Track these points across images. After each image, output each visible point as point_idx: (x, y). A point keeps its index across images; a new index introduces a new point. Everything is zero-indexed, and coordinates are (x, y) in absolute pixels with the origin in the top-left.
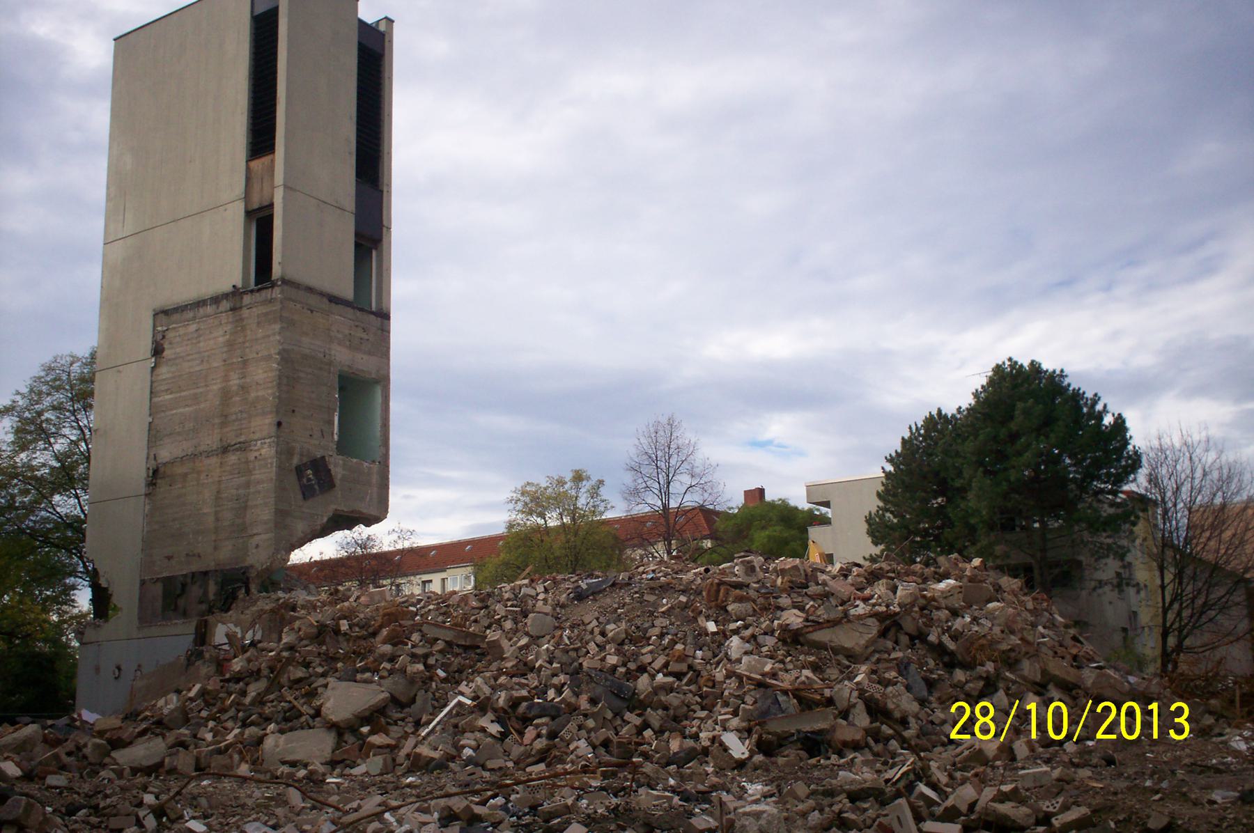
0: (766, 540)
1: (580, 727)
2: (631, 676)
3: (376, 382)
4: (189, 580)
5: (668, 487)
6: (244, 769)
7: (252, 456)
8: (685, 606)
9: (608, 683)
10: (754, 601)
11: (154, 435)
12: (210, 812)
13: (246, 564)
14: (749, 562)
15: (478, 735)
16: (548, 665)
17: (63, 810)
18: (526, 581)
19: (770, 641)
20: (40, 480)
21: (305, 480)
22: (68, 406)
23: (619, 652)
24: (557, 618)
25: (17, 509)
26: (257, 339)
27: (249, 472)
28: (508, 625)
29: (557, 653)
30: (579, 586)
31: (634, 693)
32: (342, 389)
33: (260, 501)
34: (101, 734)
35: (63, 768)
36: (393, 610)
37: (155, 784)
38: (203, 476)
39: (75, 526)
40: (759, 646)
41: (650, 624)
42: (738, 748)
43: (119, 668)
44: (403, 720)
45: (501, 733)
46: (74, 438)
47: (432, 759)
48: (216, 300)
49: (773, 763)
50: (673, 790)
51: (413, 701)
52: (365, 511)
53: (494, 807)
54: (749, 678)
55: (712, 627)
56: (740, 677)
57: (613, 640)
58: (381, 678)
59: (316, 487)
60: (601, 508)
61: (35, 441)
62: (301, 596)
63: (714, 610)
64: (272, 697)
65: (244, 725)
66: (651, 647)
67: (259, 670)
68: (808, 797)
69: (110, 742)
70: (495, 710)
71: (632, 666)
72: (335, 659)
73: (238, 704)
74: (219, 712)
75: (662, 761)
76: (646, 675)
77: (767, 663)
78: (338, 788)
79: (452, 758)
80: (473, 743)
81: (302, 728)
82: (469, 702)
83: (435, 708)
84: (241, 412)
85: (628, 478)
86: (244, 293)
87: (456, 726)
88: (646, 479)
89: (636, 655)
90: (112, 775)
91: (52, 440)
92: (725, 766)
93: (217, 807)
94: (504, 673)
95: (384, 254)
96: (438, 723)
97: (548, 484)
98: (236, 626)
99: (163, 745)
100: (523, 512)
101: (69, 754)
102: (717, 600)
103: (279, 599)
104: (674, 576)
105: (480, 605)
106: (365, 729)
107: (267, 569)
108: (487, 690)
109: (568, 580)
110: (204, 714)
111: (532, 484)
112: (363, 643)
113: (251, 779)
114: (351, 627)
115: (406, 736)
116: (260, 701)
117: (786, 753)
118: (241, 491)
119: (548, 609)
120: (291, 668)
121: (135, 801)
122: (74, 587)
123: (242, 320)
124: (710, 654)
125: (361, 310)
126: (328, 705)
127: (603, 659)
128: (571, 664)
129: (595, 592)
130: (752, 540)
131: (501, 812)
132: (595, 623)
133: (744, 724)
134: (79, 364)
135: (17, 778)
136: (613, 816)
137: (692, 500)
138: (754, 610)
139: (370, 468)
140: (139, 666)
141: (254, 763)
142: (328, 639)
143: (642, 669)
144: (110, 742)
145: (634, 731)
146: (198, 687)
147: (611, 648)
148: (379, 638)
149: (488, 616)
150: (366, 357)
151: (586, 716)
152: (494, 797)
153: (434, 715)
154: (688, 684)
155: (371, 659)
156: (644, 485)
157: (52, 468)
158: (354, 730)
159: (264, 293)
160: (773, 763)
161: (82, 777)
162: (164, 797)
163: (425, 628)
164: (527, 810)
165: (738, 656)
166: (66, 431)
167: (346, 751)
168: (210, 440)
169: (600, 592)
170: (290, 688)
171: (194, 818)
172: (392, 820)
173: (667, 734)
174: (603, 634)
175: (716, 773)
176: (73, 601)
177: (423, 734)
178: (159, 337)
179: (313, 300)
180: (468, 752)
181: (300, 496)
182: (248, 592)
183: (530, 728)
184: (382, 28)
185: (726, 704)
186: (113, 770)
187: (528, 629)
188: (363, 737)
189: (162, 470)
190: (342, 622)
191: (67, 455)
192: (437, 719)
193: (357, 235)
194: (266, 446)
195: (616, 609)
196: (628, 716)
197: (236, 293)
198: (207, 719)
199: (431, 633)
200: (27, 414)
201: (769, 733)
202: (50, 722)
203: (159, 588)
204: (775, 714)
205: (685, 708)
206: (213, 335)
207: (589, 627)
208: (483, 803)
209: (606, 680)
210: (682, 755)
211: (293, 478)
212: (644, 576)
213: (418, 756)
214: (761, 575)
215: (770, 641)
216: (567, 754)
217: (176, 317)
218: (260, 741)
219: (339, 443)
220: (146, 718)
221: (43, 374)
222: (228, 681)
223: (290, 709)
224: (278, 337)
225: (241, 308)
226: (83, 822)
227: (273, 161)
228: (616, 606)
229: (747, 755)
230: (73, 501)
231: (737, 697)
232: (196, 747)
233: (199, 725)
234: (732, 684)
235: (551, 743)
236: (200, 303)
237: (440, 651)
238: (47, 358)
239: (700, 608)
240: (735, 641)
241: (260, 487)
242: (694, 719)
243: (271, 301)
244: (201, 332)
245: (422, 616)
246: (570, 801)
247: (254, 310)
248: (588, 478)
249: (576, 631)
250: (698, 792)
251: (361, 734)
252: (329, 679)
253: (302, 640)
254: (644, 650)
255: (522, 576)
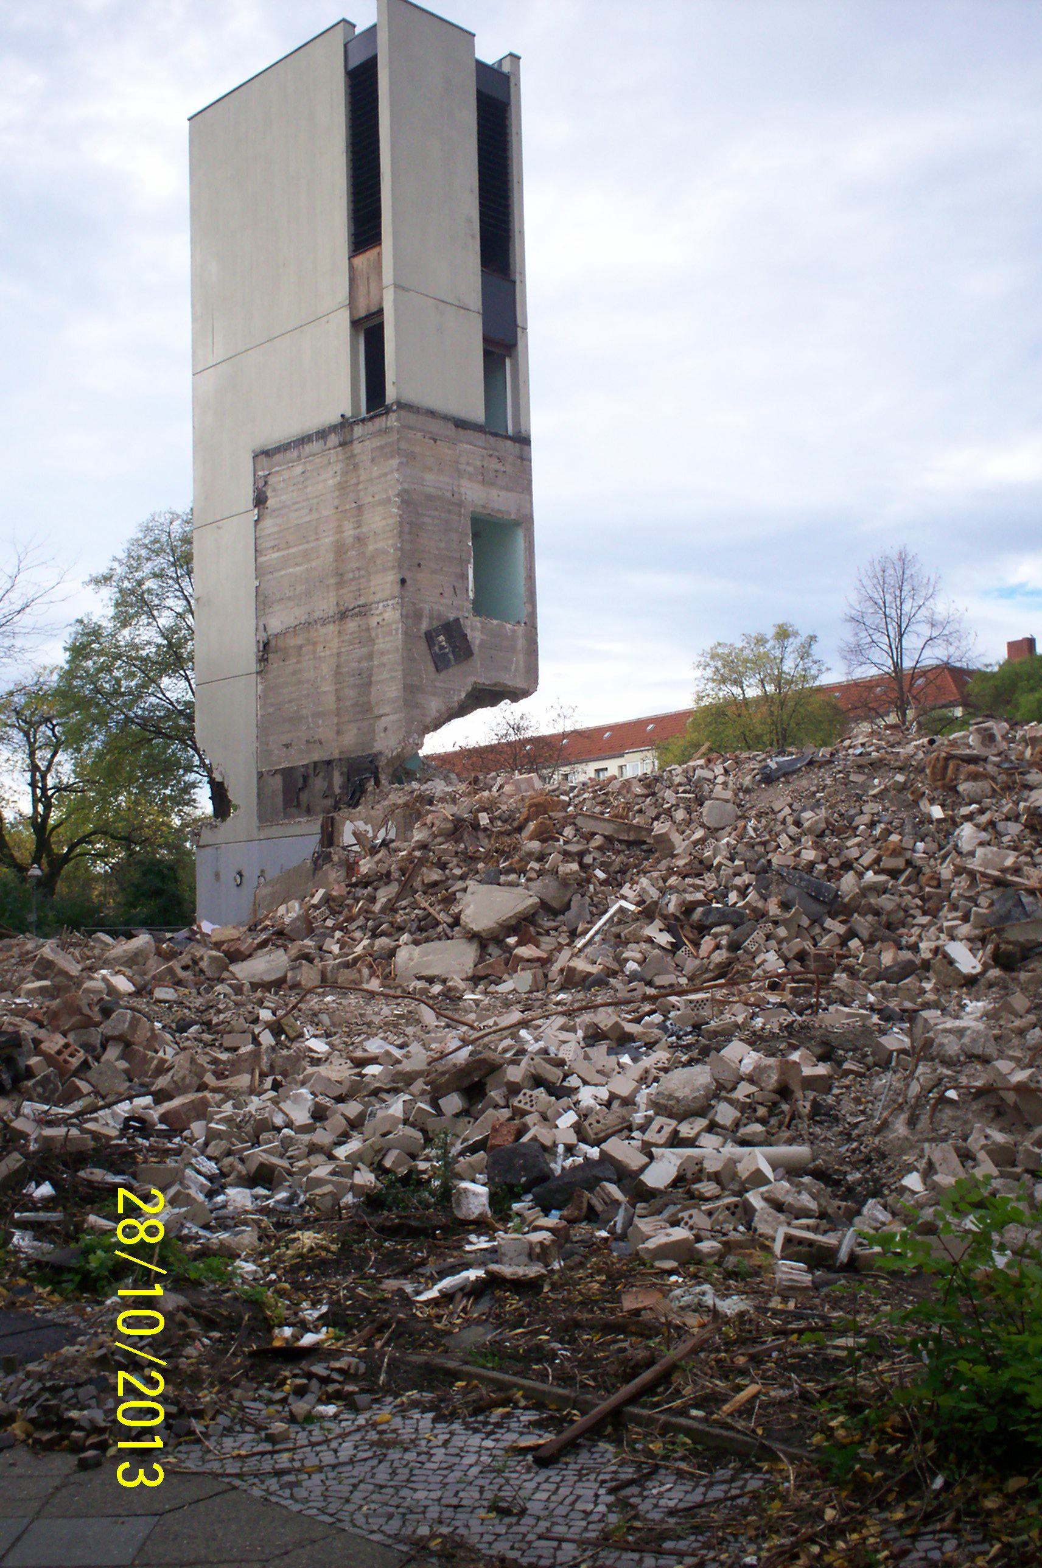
0: (1035, 705)
1: (768, 937)
2: (832, 874)
3: (517, 524)
4: (311, 771)
5: (900, 640)
6: (374, 985)
7: (373, 622)
8: (902, 788)
9: (803, 884)
10: (994, 779)
11: (263, 602)
12: (333, 1030)
13: (375, 751)
14: (986, 729)
15: (644, 946)
16: (729, 863)
17: (174, 1025)
18: (701, 762)
19: (1014, 829)
20: (145, 660)
21: (436, 648)
22: (171, 572)
23: (816, 846)
24: (739, 806)
25: (122, 694)
26: (371, 480)
27: (371, 641)
28: (680, 815)
29: (741, 848)
30: (767, 766)
31: (837, 896)
32: (476, 536)
33: (385, 675)
34: (217, 945)
35: (179, 983)
36: (541, 799)
37: (271, 1000)
38: (320, 648)
39: (187, 712)
40: (999, 835)
41: (857, 810)
42: (967, 961)
43: (240, 874)
44: (556, 929)
45: (672, 944)
46: (180, 610)
47: (589, 974)
48: (322, 434)
49: (1013, 979)
50: (872, 1008)
51: (568, 907)
52: (509, 683)
53: (650, 1025)
54: (983, 875)
55: (937, 812)
56: (972, 874)
57: (810, 831)
58: (529, 880)
59: (451, 656)
60: (813, 672)
61: (137, 614)
62: (438, 787)
63: (939, 791)
64: (404, 903)
65: (374, 936)
66: (858, 839)
67: (389, 874)
68: (1028, 1012)
69: (227, 953)
70: (664, 917)
71: (834, 862)
72: (473, 859)
73: (367, 912)
74: (346, 921)
75: (871, 977)
76: (851, 873)
77: (1008, 856)
78: (477, 1005)
79: (614, 974)
80: (639, 956)
81: (440, 939)
82: (632, 907)
83: (592, 914)
84: (358, 569)
85: (847, 635)
86: (356, 423)
87: (618, 936)
88: (871, 632)
89: (839, 849)
90: (229, 990)
91: (155, 613)
92: (950, 982)
93: (340, 1025)
94: (675, 873)
95: (520, 360)
96: (597, 933)
97: (744, 644)
98: (366, 823)
99: (285, 958)
100: (714, 680)
101: (185, 968)
102: (944, 778)
103: (412, 792)
104: (889, 750)
105: (645, 792)
106: (512, 940)
107: (398, 756)
108: (654, 893)
109: (754, 758)
110: (330, 923)
111: (725, 645)
112: (508, 840)
113: (381, 994)
114: (491, 820)
115: (559, 948)
116: (391, 908)
117: (1032, 966)
118: (365, 664)
119: (728, 794)
120: (424, 870)
121: (251, 1018)
122: (193, 785)
123: (353, 456)
124: (934, 846)
125: (495, 435)
126: (468, 912)
127: (797, 855)
128: (757, 861)
129: (786, 773)
130: (1017, 707)
131: (656, 1031)
132: (787, 810)
133: (977, 932)
134: (179, 522)
135: (130, 994)
136: (786, 1034)
137: (932, 657)
138: (994, 790)
139: (514, 631)
140: (262, 871)
141: (386, 977)
142: (466, 836)
143: (847, 866)
144: (227, 953)
145: (837, 941)
146: (321, 892)
147: (807, 841)
148: (526, 833)
149: (655, 804)
150: (503, 493)
151: (776, 923)
152: (650, 1013)
153: (592, 923)
154: (907, 882)
155: (517, 858)
156: (869, 640)
157: (158, 646)
158: (499, 941)
159: (377, 421)
160: (1013, 979)
161: (199, 993)
162: (280, 1013)
163: (579, 821)
164: (689, 1029)
165: (970, 848)
166: (170, 602)
167: (490, 965)
168: (325, 604)
169: (794, 772)
170: (425, 893)
171: (315, 1036)
172: (529, 1037)
173: (878, 946)
174: (798, 823)
175: (936, 990)
176: (194, 801)
177: (579, 945)
178: (261, 483)
179: (436, 426)
180: (632, 966)
181: (431, 667)
182: (377, 783)
183: (707, 938)
184: (506, 68)
185: (954, 908)
186: (230, 985)
187: (705, 820)
188: (509, 949)
189: (273, 643)
190: (481, 815)
191: (174, 630)
192: (596, 928)
193: (486, 340)
194: (389, 609)
195: (814, 793)
196: (829, 923)
197: (345, 424)
198: (334, 929)
199: (587, 826)
200: (126, 584)
201: (1008, 942)
202: (169, 935)
203: (277, 782)
204: (1018, 919)
205: (902, 913)
206: (321, 478)
207: (780, 816)
208: (638, 1021)
209: (801, 879)
210: (895, 969)
211: (423, 646)
212: (851, 751)
213: (572, 970)
214: (1004, 745)
215: (1014, 829)
216: (752, 968)
217: (278, 458)
218: (392, 953)
219: (475, 602)
220: (265, 928)
221: (140, 535)
222: (355, 885)
223: (425, 918)
224: (396, 476)
225: (351, 442)
226: (196, 1039)
227: (379, 254)
228: (814, 789)
229: (979, 969)
230: (183, 684)
231: (969, 898)
232: (322, 959)
233: (324, 936)
234: (963, 881)
235: (732, 955)
236: (304, 440)
237: (599, 848)
238: (144, 517)
239: (923, 789)
240: (967, 831)
241: (385, 659)
242: (914, 926)
243: (386, 431)
244: (308, 474)
245: (576, 806)
246: (740, 1020)
247: (367, 443)
248: (796, 634)
249: (763, 821)
250: (904, 1011)
251: (507, 946)
252: (469, 882)
253: (435, 837)
254: (849, 843)
255: (699, 754)
